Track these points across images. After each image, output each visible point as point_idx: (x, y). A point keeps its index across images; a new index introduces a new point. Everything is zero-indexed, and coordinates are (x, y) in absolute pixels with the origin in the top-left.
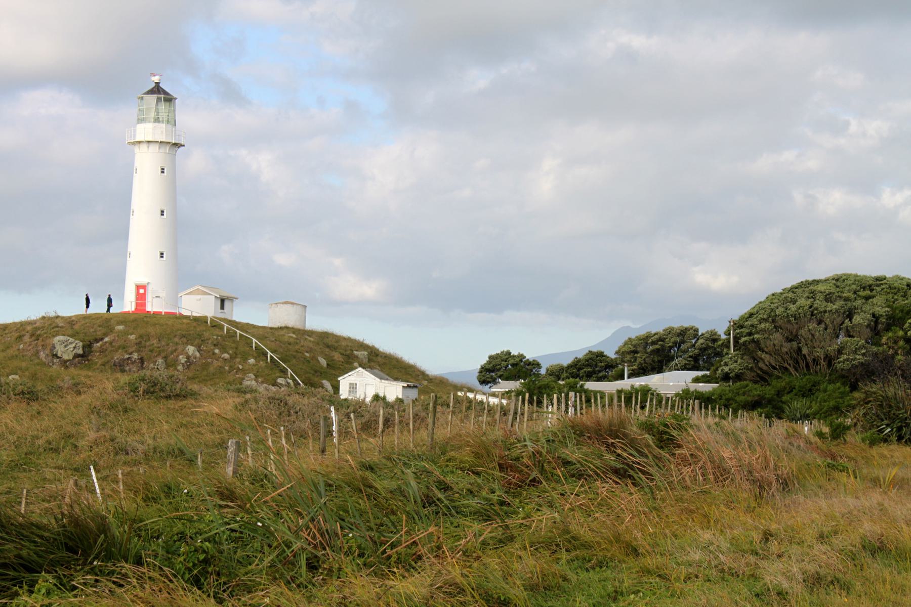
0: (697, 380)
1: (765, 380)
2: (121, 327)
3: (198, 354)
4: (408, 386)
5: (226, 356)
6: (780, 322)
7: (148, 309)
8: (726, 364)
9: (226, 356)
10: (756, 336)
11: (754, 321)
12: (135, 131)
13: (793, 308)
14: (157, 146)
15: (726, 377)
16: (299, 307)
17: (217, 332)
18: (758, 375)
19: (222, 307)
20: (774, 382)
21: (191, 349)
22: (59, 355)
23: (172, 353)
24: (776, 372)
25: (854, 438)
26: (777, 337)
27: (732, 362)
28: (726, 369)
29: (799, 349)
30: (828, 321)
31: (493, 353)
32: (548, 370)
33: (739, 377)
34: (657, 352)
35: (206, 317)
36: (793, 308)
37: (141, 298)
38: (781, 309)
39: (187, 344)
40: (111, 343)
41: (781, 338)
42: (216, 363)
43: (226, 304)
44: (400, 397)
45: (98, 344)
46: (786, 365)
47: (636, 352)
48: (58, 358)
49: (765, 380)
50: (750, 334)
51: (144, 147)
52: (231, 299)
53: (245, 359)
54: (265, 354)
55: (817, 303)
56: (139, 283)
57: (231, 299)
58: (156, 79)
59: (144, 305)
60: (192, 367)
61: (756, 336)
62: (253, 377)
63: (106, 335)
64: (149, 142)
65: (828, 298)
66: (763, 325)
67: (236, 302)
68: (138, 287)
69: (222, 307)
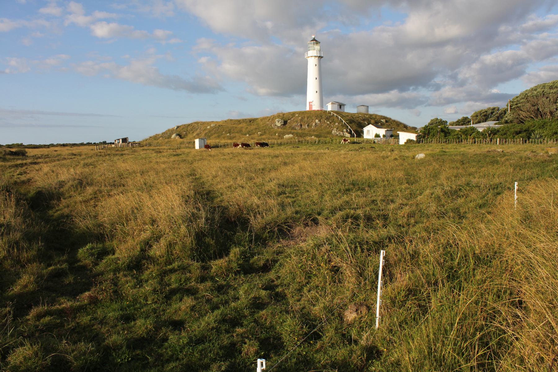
0: (496, 124)
1: (523, 123)
5: (328, 123)
6: (529, 98)
8: (506, 117)
9: (328, 123)
10: (519, 105)
11: (519, 99)
13: (535, 92)
15: (506, 122)
18: (520, 121)
19: (340, 108)
20: (526, 123)
21: (317, 121)
24: (527, 119)
25: (209, 184)
26: (528, 105)
27: (509, 116)
28: (507, 119)
29: (538, 109)
30: (551, 97)
33: (511, 122)
34: (485, 115)
36: (535, 92)
37: (311, 106)
38: (530, 93)
41: (530, 105)
42: (325, 125)
43: (342, 107)
46: (532, 116)
47: (477, 116)
49: (523, 123)
50: (517, 104)
52: (344, 105)
55: (546, 90)
57: (344, 105)
58: (313, 37)
61: (519, 105)
65: (551, 88)
66: (522, 101)
69: (340, 108)
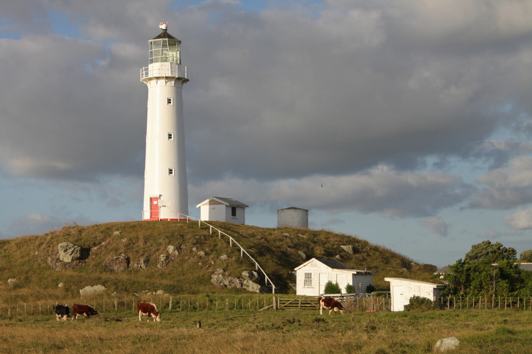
2: (117, 233)
3: (176, 253)
9: (202, 253)
12: (147, 69)
14: (163, 81)
16: (301, 212)
17: (205, 232)
19: (234, 214)
21: (171, 248)
22: (61, 259)
23: (155, 252)
31: (476, 243)
32: (521, 255)
35: (514, 252)
37: (154, 209)
40: (106, 247)
42: (192, 260)
43: (238, 211)
45: (95, 248)
48: (61, 261)
51: (154, 82)
52: (243, 207)
53: (219, 255)
54: (239, 250)
56: (152, 196)
57: (243, 207)
59: (157, 214)
60: (170, 264)
62: (222, 271)
63: (103, 240)
64: (166, 78)
67: (246, 210)
68: (151, 200)
69: (234, 214)
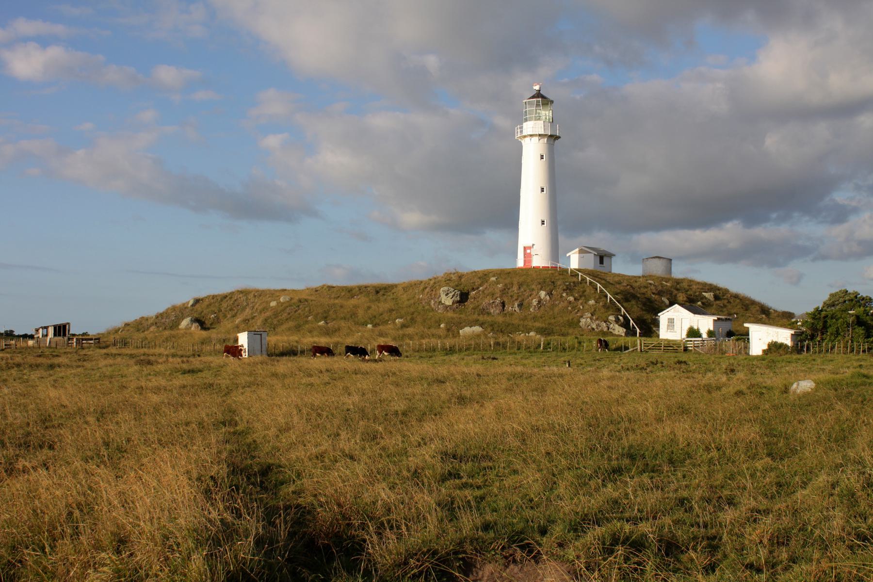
2: (493, 279)
3: (548, 297)
4: (719, 319)
7: (613, 271)
9: (571, 298)
14: (537, 138)
16: (665, 261)
19: (601, 262)
21: (543, 294)
23: (528, 297)
25: (267, 448)
37: (527, 257)
39: (541, 289)
40: (483, 291)
43: (605, 259)
44: (712, 329)
52: (610, 256)
53: (587, 300)
54: (606, 296)
57: (610, 256)
58: (537, 88)
59: (530, 261)
60: (542, 308)
62: (590, 315)
63: (481, 285)
67: (613, 259)
68: (525, 248)
69: (601, 262)
